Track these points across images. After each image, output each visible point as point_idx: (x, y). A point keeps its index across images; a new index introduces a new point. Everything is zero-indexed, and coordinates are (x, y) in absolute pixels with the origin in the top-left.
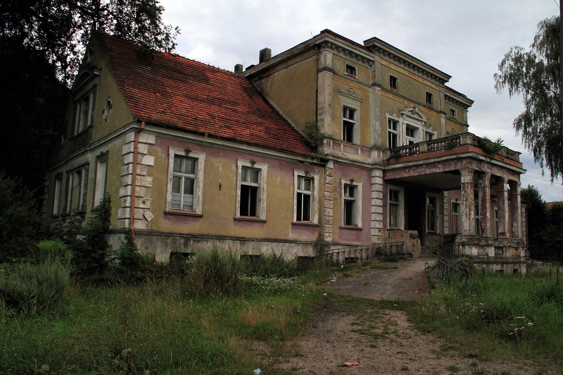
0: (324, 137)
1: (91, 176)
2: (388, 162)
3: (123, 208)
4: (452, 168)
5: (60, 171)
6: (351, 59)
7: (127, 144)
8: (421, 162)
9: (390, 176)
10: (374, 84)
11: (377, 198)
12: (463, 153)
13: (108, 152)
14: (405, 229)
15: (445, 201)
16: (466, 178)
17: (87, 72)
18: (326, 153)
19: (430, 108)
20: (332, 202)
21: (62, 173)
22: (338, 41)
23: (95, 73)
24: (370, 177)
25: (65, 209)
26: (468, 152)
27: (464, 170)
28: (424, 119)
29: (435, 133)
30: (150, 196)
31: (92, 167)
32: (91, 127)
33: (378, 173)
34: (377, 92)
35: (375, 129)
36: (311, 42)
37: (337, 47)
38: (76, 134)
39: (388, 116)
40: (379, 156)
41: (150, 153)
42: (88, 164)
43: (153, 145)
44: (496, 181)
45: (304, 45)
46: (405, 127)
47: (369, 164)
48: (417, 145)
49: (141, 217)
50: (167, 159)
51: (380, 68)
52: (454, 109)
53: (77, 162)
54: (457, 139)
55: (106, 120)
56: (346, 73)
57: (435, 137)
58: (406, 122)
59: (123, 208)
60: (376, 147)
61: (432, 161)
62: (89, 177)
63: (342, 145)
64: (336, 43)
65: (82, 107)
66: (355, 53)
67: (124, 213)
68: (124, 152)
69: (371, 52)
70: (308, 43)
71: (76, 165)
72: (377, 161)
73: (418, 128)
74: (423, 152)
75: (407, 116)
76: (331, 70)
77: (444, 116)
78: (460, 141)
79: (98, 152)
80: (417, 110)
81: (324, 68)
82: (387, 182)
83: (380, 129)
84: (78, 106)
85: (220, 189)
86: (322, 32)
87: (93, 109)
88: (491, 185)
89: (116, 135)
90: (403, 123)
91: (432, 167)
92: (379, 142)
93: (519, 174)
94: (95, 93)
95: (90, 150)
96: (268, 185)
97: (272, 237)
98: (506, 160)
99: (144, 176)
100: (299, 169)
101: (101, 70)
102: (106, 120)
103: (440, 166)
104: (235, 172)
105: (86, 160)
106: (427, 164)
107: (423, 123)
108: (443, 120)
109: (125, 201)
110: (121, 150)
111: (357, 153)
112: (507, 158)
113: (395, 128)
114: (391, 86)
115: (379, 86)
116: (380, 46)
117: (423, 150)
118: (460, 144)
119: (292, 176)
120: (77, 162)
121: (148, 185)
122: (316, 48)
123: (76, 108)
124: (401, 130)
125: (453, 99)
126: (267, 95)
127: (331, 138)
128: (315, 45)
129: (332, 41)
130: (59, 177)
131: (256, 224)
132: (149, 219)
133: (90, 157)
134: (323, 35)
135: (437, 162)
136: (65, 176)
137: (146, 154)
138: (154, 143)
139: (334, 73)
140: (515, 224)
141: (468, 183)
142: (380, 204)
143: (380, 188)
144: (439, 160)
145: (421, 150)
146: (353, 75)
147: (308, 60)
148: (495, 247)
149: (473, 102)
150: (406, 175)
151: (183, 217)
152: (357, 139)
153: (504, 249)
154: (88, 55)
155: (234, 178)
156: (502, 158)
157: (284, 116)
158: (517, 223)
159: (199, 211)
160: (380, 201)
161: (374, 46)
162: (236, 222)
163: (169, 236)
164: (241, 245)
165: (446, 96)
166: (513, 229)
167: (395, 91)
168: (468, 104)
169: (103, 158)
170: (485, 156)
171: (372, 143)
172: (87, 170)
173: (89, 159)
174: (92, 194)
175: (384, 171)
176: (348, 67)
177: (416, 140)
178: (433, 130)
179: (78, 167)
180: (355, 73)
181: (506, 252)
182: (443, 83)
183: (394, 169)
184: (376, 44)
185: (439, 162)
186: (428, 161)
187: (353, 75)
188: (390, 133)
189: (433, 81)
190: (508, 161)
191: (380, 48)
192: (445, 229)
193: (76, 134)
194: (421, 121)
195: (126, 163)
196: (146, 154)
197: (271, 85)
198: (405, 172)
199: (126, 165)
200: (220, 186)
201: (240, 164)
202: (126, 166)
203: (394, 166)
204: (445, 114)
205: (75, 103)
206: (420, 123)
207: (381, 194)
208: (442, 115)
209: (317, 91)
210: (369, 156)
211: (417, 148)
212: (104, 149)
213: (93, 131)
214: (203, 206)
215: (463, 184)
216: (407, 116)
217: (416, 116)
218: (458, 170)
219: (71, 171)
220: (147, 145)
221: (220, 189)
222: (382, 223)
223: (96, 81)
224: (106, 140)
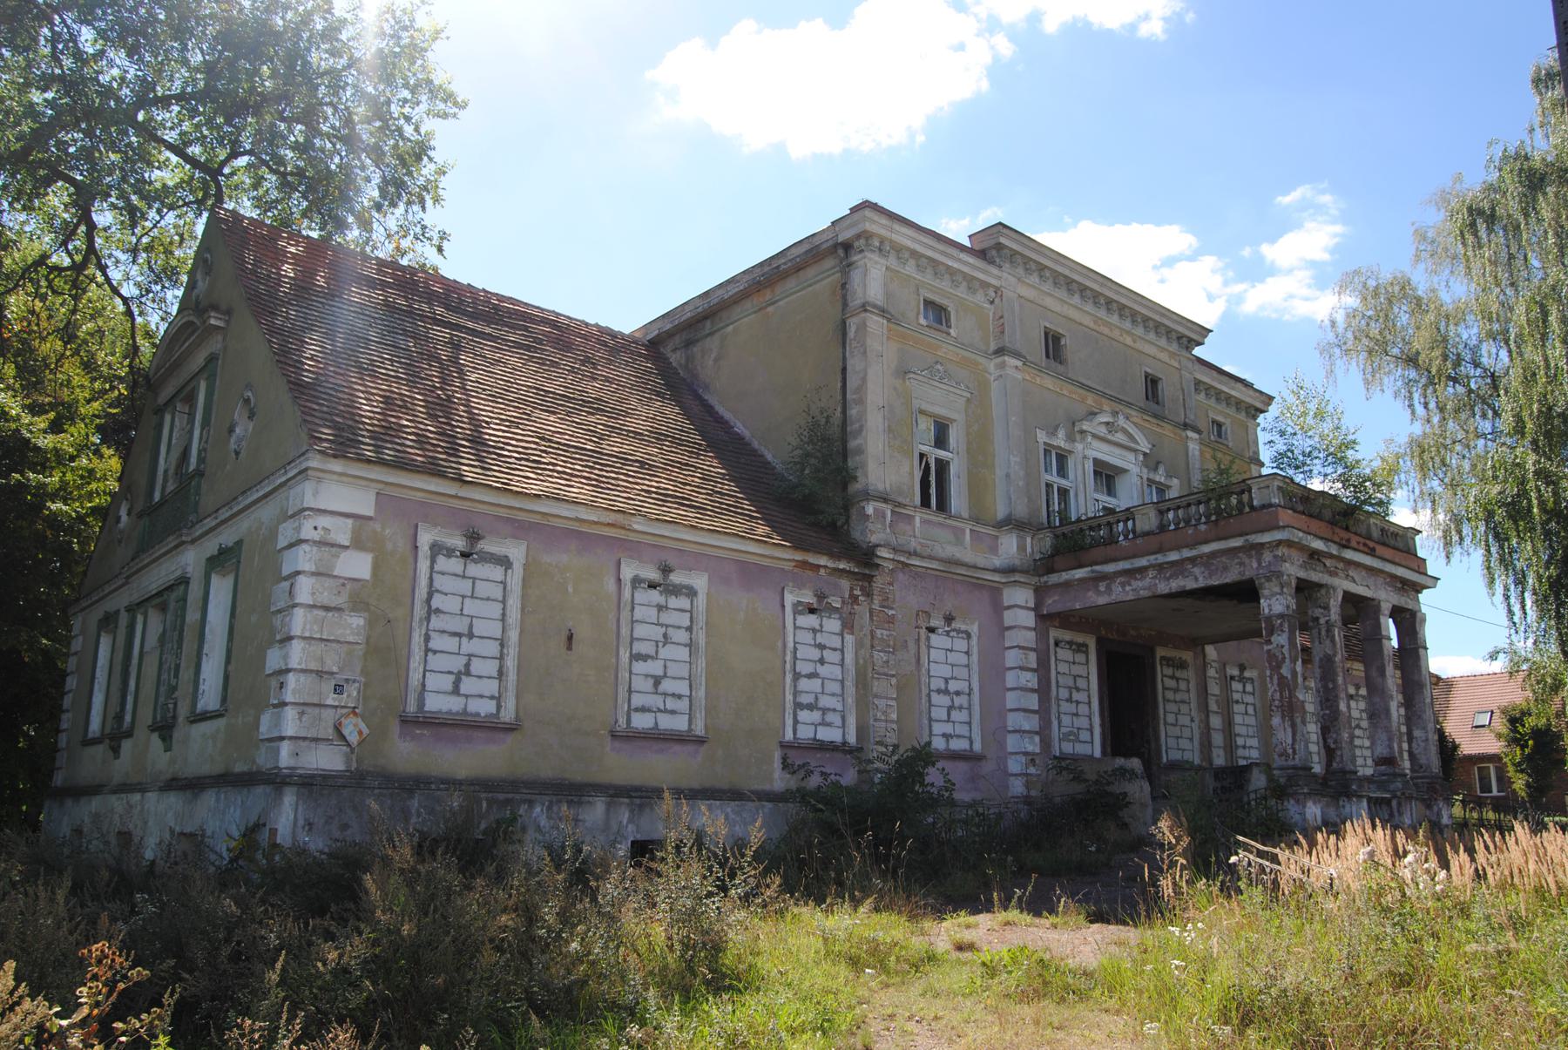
0: (867, 495)
1: (192, 616)
2: (1046, 565)
3: (275, 706)
4: (1231, 577)
5: (109, 606)
6: (936, 283)
7: (292, 516)
8: (1143, 562)
9: (1053, 603)
10: (1000, 351)
11: (1022, 668)
12: (1262, 531)
13: (239, 543)
14: (1104, 752)
15: (1211, 672)
16: (1275, 603)
17: (192, 323)
18: (874, 539)
19: (1155, 416)
20: (894, 681)
21: (117, 612)
22: (898, 233)
23: (213, 322)
24: (998, 608)
25: (119, 717)
26: (1278, 528)
27: (1269, 579)
28: (1145, 446)
29: (1175, 482)
30: (358, 670)
31: (195, 590)
32: (199, 473)
33: (1020, 596)
34: (1010, 371)
35: (1008, 475)
36: (825, 237)
37: (898, 249)
38: (157, 496)
39: (1042, 437)
40: (1022, 548)
41: (358, 544)
42: (184, 581)
43: (370, 518)
44: (1359, 610)
45: (806, 247)
46: (1089, 467)
47: (995, 570)
48: (1129, 514)
49: (330, 732)
50: (411, 560)
51: (1017, 308)
52: (1220, 419)
53: (157, 577)
54: (1243, 492)
55: (237, 453)
56: (922, 321)
57: (1173, 494)
58: (1092, 454)
59: (275, 706)
60: (1011, 523)
61: (1173, 556)
62: (188, 619)
63: (917, 520)
64: (894, 237)
65: (177, 423)
66: (948, 267)
67: (277, 722)
68: (282, 543)
69: (992, 262)
70: (817, 241)
71: (154, 586)
72: (1017, 562)
73: (1126, 471)
74: (1147, 534)
75: (1095, 436)
76: (883, 312)
77: (1195, 436)
78: (1251, 498)
79: (211, 547)
80: (1121, 421)
81: (863, 305)
82: (1045, 619)
83: (1022, 473)
84: (168, 418)
85: (569, 648)
86: (854, 210)
87: (206, 423)
88: (1346, 621)
89: (261, 493)
90: (1085, 457)
91: (1174, 576)
92: (1021, 511)
93: (1418, 588)
94: (211, 379)
95: (193, 542)
96: (708, 635)
97: (723, 784)
98: (1380, 550)
99: (338, 609)
100: (800, 585)
101: (229, 312)
102: (237, 453)
103: (1197, 571)
104: (615, 599)
105: (178, 573)
106: (1160, 567)
107: (1141, 458)
108: (1194, 447)
109: (282, 685)
110: (273, 534)
111: (959, 541)
112: (1384, 544)
113: (1062, 472)
114: (1048, 356)
115: (1017, 354)
116: (1014, 246)
117: (1147, 528)
118: (1252, 508)
119: (778, 607)
120: (157, 577)
121: (351, 639)
122: (841, 252)
123: (160, 426)
124: (1080, 477)
125: (1219, 393)
126: (706, 387)
127: (885, 500)
128: (836, 246)
129: (883, 232)
130: (108, 622)
131: (677, 748)
132: (354, 739)
133: (191, 560)
134: (856, 216)
135: (1188, 559)
136: (124, 619)
137: (347, 547)
138: (371, 513)
139: (889, 320)
140: (1417, 733)
141: (1281, 616)
142: (1030, 685)
143: (1029, 638)
144: (1193, 553)
145: (1138, 529)
146: (944, 327)
147: (817, 286)
148: (1370, 800)
149: (1271, 398)
150: (1102, 600)
151: (459, 732)
152: (958, 499)
153: (1394, 803)
154: (199, 276)
155: (612, 616)
156: (1371, 544)
157: (756, 444)
158: (1424, 728)
159: (699, 729)
160: (1029, 675)
161: (999, 247)
162: (617, 744)
163: (411, 792)
164: (632, 811)
165: (1198, 383)
166: (1414, 745)
167: (1061, 368)
168: (1259, 405)
169: (223, 560)
170: (1326, 540)
171: (1001, 514)
172: (184, 600)
173: (190, 569)
174: (192, 671)
175: (1040, 592)
176: (929, 303)
177: (1122, 502)
178: (1169, 476)
179: (159, 594)
180: (948, 321)
181: (1400, 814)
182: (1189, 349)
183: (1067, 585)
184: (1002, 240)
185: (1192, 560)
186: (1160, 558)
187: (944, 327)
188: (1049, 486)
189: (1163, 342)
190: (1387, 553)
191: (1015, 253)
192: (1215, 752)
193: (157, 496)
194: (1135, 451)
195: (285, 573)
196: (347, 547)
197: (716, 360)
198: (1099, 593)
199: (285, 579)
200: (570, 638)
201: (628, 572)
202: (286, 584)
203: (1065, 576)
204: (1199, 432)
205: (160, 411)
206: (1131, 456)
207: (1033, 656)
208: (1190, 434)
209: (844, 369)
210: (994, 549)
211: (1130, 523)
212: (227, 537)
213: (204, 487)
214: (518, 697)
215: (1269, 619)
216: (1095, 436)
217: (1119, 437)
218: (1251, 581)
219: (139, 604)
220: (350, 521)
221: (569, 648)
222: (1037, 739)
223: (215, 345)
224: (235, 509)
